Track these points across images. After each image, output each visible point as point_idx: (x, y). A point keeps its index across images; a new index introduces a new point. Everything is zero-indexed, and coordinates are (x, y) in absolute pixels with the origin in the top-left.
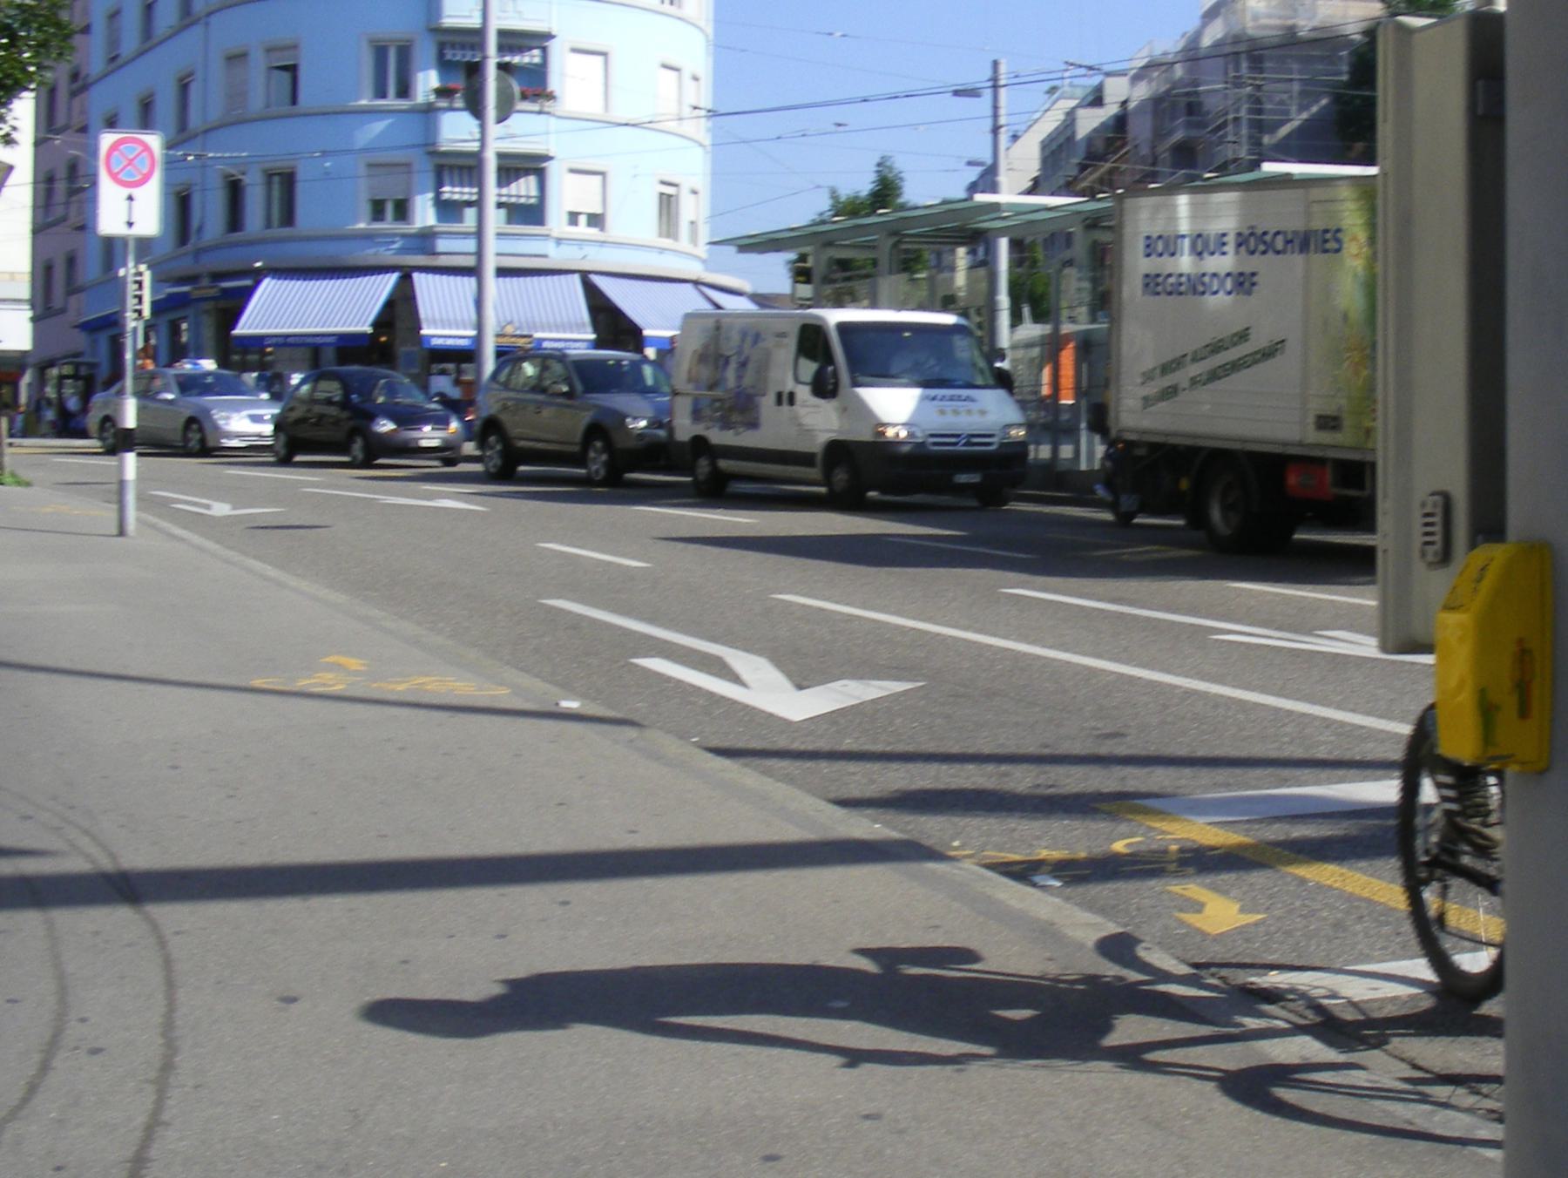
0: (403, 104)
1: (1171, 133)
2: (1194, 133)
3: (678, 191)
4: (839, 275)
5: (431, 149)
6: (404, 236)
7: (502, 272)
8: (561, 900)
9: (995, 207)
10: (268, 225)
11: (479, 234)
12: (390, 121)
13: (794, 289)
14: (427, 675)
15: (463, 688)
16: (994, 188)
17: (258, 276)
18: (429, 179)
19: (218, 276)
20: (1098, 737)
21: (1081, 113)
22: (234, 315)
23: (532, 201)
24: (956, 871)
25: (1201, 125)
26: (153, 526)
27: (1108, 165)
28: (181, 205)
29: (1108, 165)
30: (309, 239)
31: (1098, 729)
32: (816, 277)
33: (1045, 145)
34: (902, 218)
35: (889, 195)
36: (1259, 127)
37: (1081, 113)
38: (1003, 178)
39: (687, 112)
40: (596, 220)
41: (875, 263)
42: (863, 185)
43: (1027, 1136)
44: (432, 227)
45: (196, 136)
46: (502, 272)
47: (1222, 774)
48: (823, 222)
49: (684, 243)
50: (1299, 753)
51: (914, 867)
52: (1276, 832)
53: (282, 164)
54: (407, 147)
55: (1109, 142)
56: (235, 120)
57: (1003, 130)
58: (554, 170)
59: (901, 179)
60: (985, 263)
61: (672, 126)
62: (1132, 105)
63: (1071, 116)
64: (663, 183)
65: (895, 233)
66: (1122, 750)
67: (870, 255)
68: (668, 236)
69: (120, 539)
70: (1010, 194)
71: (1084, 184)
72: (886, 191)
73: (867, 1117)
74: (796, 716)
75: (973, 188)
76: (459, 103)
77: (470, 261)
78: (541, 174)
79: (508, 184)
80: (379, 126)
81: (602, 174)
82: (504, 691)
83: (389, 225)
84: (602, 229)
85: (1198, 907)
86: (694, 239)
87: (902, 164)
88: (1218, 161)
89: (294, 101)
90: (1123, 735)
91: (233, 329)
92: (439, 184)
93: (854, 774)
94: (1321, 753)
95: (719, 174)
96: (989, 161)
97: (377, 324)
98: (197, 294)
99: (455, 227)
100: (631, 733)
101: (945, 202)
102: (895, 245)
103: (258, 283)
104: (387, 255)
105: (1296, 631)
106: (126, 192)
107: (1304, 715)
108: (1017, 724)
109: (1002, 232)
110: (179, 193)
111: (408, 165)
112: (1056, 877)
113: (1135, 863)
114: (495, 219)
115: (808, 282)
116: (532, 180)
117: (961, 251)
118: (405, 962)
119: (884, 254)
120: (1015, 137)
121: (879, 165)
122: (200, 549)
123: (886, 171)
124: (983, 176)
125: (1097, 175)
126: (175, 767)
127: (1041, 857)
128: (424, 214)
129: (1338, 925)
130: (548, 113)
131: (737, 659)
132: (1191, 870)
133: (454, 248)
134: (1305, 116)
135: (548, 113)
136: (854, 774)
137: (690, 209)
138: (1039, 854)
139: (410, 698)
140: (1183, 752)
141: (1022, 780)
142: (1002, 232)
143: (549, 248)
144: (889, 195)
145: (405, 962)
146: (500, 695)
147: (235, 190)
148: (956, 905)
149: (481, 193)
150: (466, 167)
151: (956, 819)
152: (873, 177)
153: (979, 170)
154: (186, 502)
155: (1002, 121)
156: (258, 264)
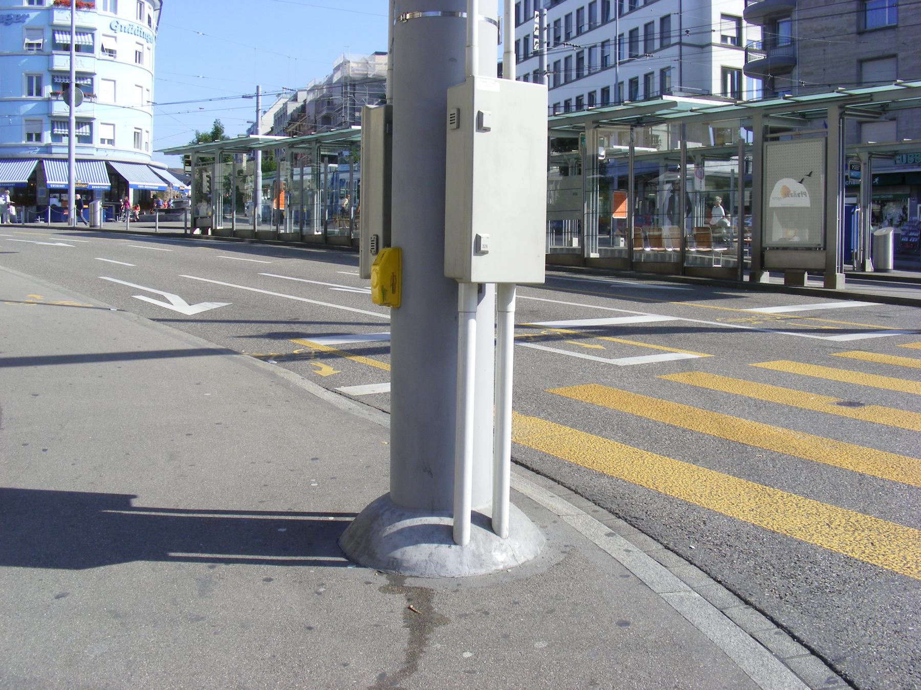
0: (39, 98)
1: (321, 112)
2: (330, 112)
4: (201, 163)
6: (39, 147)
7: (77, 160)
9: (258, 139)
11: (69, 147)
18: (50, 126)
23: (88, 134)
25: (332, 109)
32: (193, 164)
33: (275, 116)
40: (111, 142)
41: (214, 159)
42: (209, 130)
46: (77, 160)
49: (144, 151)
51: (230, 356)
58: (96, 124)
60: (253, 159)
63: (285, 105)
64: (136, 128)
65: (222, 148)
67: (211, 156)
72: (217, 133)
77: (67, 156)
78: (91, 125)
80: (30, 106)
81: (114, 125)
83: (34, 143)
86: (147, 149)
87: (223, 122)
92: (53, 128)
95: (156, 126)
97: (28, 180)
102: (221, 153)
104: (34, 154)
109: (259, 148)
113: (300, 357)
115: (190, 165)
116: (88, 127)
117: (245, 155)
120: (265, 112)
124: (252, 126)
128: (47, 138)
131: (168, 296)
133: (59, 151)
137: (145, 138)
142: (259, 148)
143: (94, 152)
148: (243, 367)
149: (70, 132)
150: (64, 122)
152: (213, 127)
155: (260, 108)
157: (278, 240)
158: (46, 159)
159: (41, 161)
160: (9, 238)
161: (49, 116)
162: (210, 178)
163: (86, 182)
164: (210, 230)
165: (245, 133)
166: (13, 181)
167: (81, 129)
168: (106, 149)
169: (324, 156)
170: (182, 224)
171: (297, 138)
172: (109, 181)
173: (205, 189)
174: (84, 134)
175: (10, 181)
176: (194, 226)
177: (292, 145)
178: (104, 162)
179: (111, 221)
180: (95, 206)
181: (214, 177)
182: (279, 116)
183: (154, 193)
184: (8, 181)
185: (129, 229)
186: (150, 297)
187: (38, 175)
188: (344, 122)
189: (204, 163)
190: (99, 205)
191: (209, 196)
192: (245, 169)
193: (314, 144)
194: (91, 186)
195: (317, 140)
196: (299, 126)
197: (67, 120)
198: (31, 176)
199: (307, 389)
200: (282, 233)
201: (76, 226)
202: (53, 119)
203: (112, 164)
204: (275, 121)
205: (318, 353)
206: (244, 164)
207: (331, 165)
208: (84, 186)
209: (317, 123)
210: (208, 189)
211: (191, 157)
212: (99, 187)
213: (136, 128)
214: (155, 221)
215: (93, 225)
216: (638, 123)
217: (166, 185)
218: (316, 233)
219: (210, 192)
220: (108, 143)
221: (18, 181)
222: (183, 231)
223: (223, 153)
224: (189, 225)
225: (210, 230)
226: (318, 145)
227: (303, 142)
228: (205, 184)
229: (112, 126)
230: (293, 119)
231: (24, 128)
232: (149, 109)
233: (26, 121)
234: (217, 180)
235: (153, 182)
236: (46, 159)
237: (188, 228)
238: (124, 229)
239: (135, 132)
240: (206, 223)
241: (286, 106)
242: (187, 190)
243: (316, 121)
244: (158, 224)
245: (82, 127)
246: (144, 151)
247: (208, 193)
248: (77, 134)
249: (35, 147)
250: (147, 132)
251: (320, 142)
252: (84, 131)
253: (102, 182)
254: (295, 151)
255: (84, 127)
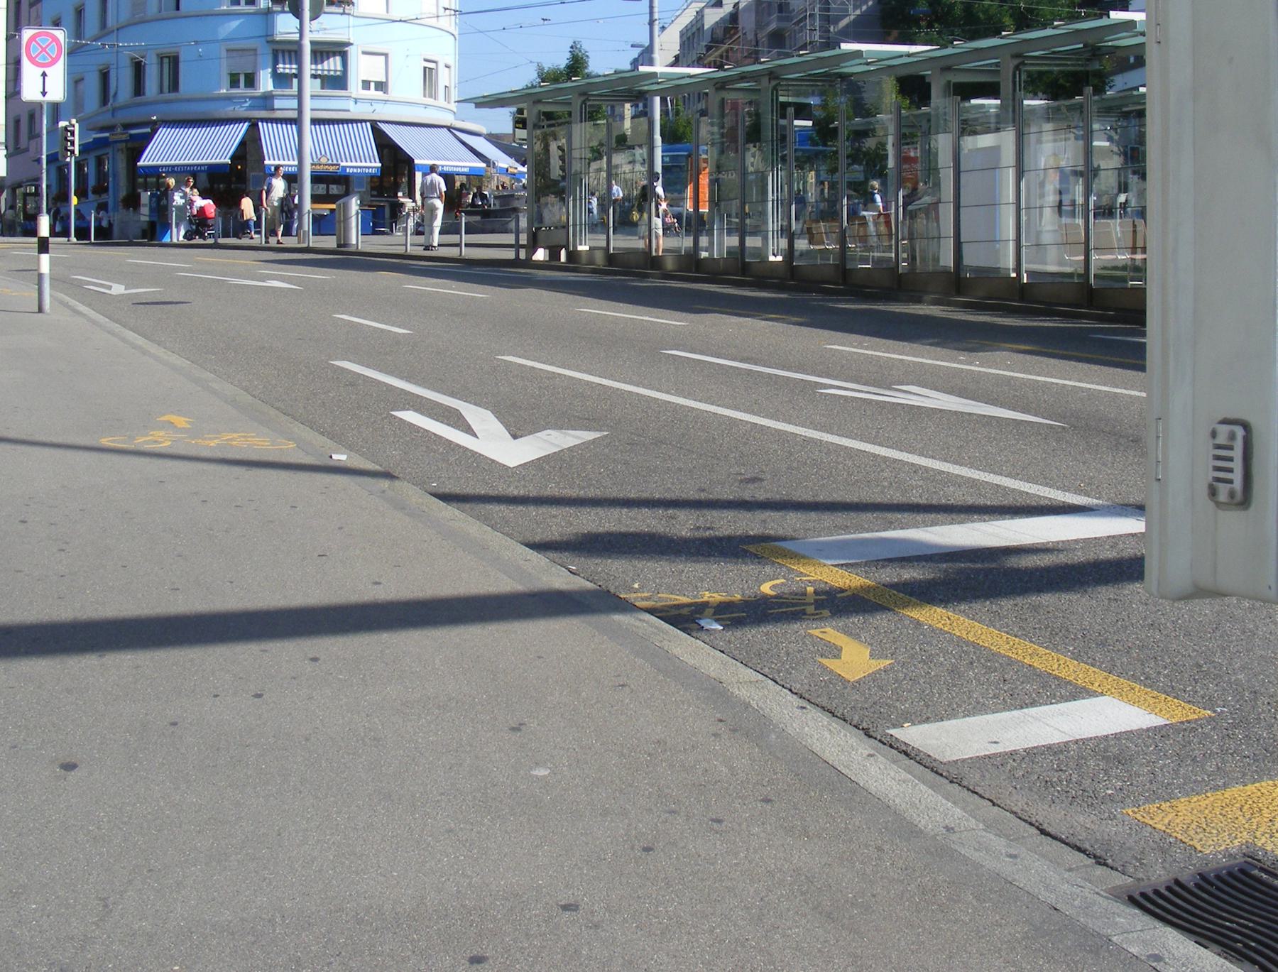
0: (251, 9)
1: (768, 24)
2: (784, 25)
3: (437, 66)
4: (546, 123)
5: (269, 39)
6: (251, 98)
7: (315, 122)
8: (311, 656)
9: (654, 75)
10: (161, 91)
11: (300, 97)
12: (242, 20)
13: (514, 131)
14: (235, 432)
15: (259, 443)
16: (651, 63)
17: (155, 127)
18: (270, 58)
19: (127, 126)
20: (741, 481)
21: (707, 11)
22: (139, 153)
23: (338, 73)
24: (638, 623)
25: (788, 19)
26: (67, 305)
27: (726, 46)
28: (75, 82)
29: (726, 46)
30: (189, 100)
31: (741, 474)
32: (529, 124)
33: (682, 34)
34: (588, 83)
35: (578, 68)
36: (827, 20)
37: (707, 11)
38: (656, 55)
39: (441, 11)
40: (381, 86)
41: (570, 114)
42: (561, 60)
43: (712, 931)
44: (272, 91)
45: (113, 31)
46: (315, 122)
47: (841, 518)
48: (533, 87)
49: (441, 101)
50: (897, 498)
51: (602, 619)
52: (890, 575)
53: (170, 50)
54: (252, 38)
55: (726, 30)
56: (138, 21)
57: (657, 22)
58: (352, 52)
59: (587, 56)
60: (646, 113)
61: (433, 22)
62: (741, 6)
63: (700, 14)
64: (426, 60)
65: (584, 94)
66: (761, 496)
67: (566, 109)
68: (431, 96)
69: (40, 314)
70: (661, 66)
71: (711, 58)
72: (576, 64)
73: (566, 908)
74: (512, 463)
75: (635, 63)
76: (287, 9)
77: (294, 115)
78: (344, 56)
79: (322, 62)
80: (235, 24)
81: (386, 55)
82: (292, 445)
83: (241, 90)
84: (386, 92)
85: (836, 652)
86: (447, 98)
87: (586, 46)
88: (800, 44)
89: (178, 8)
90: (761, 480)
91: (139, 161)
92: (276, 62)
93: (555, 517)
94: (915, 499)
95: (463, 55)
96: (647, 44)
97: (232, 158)
98: (116, 138)
99: (287, 92)
100: (385, 484)
101: (616, 72)
102: (584, 102)
103: (154, 132)
104: (241, 111)
105: (880, 387)
106: (41, 70)
107: (895, 461)
108: (680, 469)
109: (656, 92)
110: (100, 71)
111: (255, 50)
112: (717, 620)
113: (781, 605)
114: (311, 86)
115: (524, 127)
116: (338, 59)
117: (628, 106)
118: (175, 724)
119: (576, 108)
120: (663, 28)
121: (572, 47)
122: (94, 322)
123: (577, 51)
124: (641, 54)
125: (717, 53)
126: (24, 522)
127: (705, 599)
128: (265, 83)
129: (953, 671)
130: (349, 14)
131: (471, 412)
132: (826, 613)
133: (285, 105)
134: (858, 12)
135: (349, 14)
136: (555, 517)
137: (444, 77)
138: (702, 596)
139: (219, 455)
140: (807, 497)
141: (684, 525)
142: (656, 92)
143: (350, 105)
144: (578, 68)
145: (175, 724)
146: (287, 450)
147: (138, 69)
148: (639, 661)
149: (300, 69)
150: (291, 51)
151: (635, 562)
152: (568, 55)
153: (639, 50)
154: (94, 283)
155: (656, 16)
156: (155, 118)
157: (697, 271)
158: (263, 120)
159: (254, 126)
160: (184, 270)
161: (268, 42)
162: (563, 151)
163: (335, 162)
164: (563, 252)
165: (628, 67)
166: (204, 161)
167: (326, 63)
168: (371, 101)
169: (784, 106)
170: (509, 239)
171: (730, 71)
172: (377, 160)
173: (556, 172)
174: (332, 73)
175: (200, 161)
176: (533, 246)
177: (721, 85)
178: (368, 124)
179: (383, 233)
180: (346, 208)
181: (570, 150)
182: (689, 34)
183: (464, 179)
184: (195, 161)
185: (411, 250)
186: (430, 416)
187: (249, 150)
188: (811, 43)
189: (553, 122)
190: (354, 204)
191: (562, 184)
192: (629, 133)
193: (765, 80)
194: (344, 168)
195: (772, 74)
196: (727, 51)
197: (295, 47)
198: (237, 149)
199: (817, 749)
200: (705, 259)
201: (311, 245)
202: (276, 47)
203: (383, 127)
204: (682, 45)
205: (826, 593)
206: (627, 124)
207: (797, 122)
208: (332, 169)
209: (760, 43)
210: (561, 173)
211: (525, 112)
212: (359, 170)
213: (426, 60)
214: (458, 232)
215: (343, 244)
216: (1094, 55)
217: (484, 165)
218: (772, 258)
219: (563, 178)
220: (376, 89)
221: (213, 161)
222: (509, 254)
223: (588, 103)
224: (523, 239)
225: (563, 252)
226: (774, 83)
227: (743, 77)
228: (555, 163)
229: (383, 58)
230: (715, 41)
231: (224, 63)
232: (449, 23)
233: (228, 51)
234: (576, 154)
235: (460, 160)
236: (263, 120)
237: (523, 246)
238: (400, 250)
239: (425, 68)
240: (558, 237)
241: (703, 16)
242: (522, 173)
243: (757, 42)
244: (465, 238)
245: (328, 58)
246: (441, 101)
247: (560, 178)
248: (313, 72)
249: (244, 98)
250: (447, 67)
251: (777, 78)
252: (332, 68)
253: (367, 162)
254: (730, 96)
255: (331, 59)
